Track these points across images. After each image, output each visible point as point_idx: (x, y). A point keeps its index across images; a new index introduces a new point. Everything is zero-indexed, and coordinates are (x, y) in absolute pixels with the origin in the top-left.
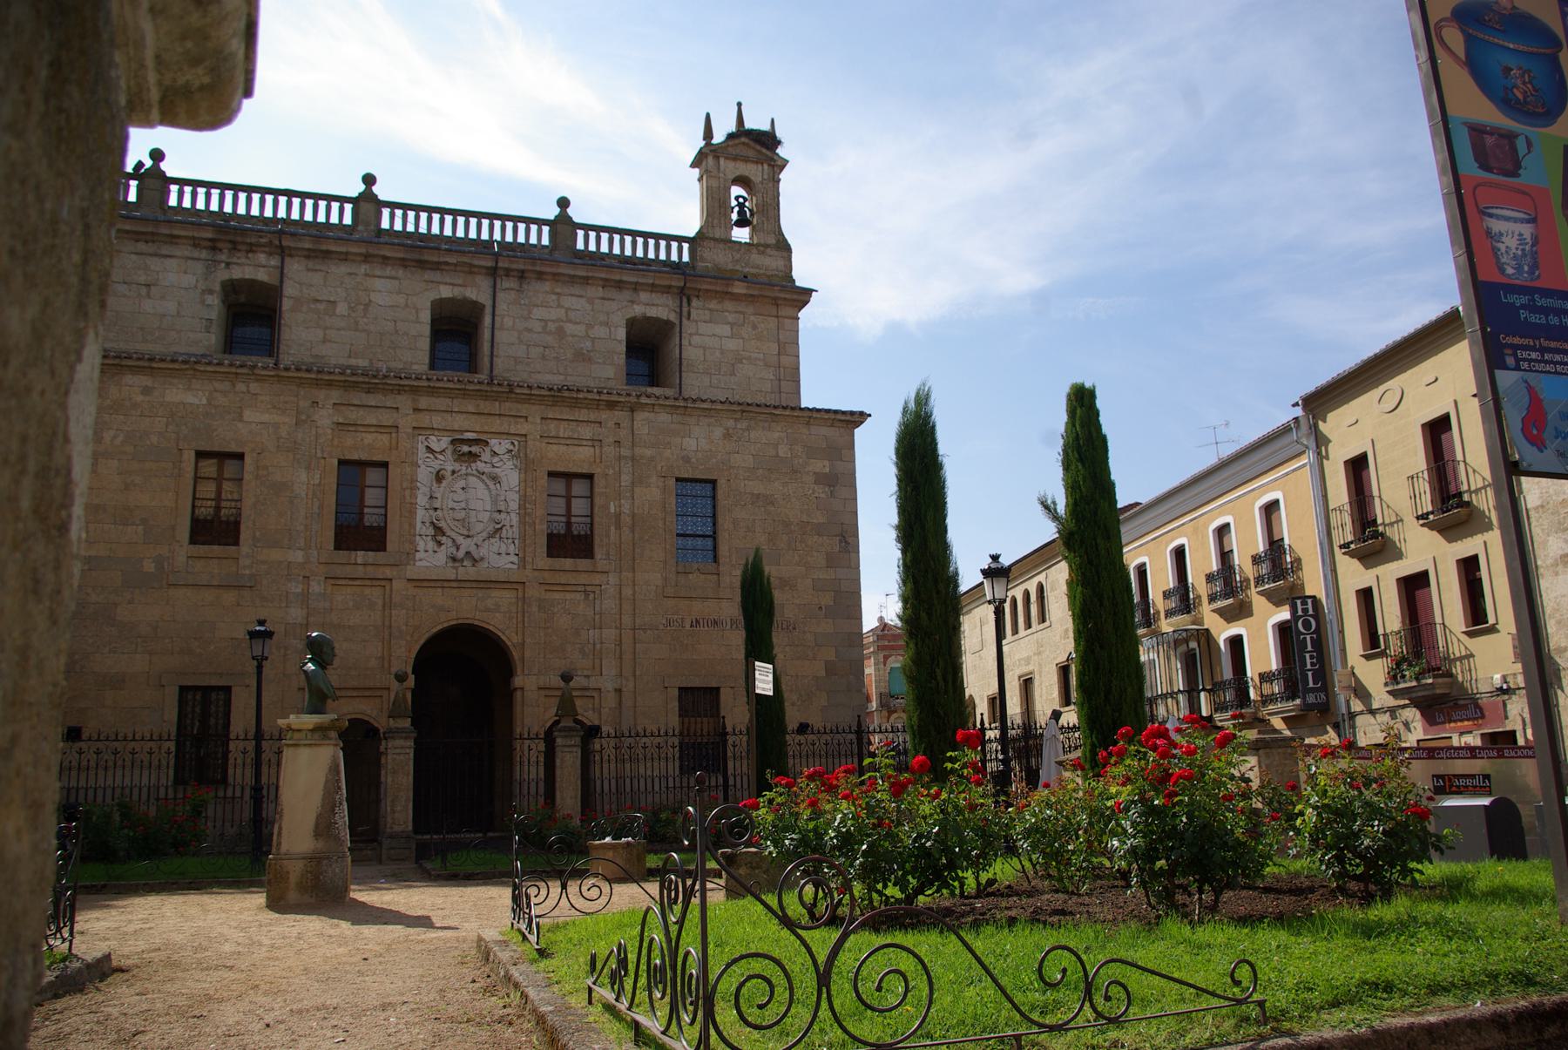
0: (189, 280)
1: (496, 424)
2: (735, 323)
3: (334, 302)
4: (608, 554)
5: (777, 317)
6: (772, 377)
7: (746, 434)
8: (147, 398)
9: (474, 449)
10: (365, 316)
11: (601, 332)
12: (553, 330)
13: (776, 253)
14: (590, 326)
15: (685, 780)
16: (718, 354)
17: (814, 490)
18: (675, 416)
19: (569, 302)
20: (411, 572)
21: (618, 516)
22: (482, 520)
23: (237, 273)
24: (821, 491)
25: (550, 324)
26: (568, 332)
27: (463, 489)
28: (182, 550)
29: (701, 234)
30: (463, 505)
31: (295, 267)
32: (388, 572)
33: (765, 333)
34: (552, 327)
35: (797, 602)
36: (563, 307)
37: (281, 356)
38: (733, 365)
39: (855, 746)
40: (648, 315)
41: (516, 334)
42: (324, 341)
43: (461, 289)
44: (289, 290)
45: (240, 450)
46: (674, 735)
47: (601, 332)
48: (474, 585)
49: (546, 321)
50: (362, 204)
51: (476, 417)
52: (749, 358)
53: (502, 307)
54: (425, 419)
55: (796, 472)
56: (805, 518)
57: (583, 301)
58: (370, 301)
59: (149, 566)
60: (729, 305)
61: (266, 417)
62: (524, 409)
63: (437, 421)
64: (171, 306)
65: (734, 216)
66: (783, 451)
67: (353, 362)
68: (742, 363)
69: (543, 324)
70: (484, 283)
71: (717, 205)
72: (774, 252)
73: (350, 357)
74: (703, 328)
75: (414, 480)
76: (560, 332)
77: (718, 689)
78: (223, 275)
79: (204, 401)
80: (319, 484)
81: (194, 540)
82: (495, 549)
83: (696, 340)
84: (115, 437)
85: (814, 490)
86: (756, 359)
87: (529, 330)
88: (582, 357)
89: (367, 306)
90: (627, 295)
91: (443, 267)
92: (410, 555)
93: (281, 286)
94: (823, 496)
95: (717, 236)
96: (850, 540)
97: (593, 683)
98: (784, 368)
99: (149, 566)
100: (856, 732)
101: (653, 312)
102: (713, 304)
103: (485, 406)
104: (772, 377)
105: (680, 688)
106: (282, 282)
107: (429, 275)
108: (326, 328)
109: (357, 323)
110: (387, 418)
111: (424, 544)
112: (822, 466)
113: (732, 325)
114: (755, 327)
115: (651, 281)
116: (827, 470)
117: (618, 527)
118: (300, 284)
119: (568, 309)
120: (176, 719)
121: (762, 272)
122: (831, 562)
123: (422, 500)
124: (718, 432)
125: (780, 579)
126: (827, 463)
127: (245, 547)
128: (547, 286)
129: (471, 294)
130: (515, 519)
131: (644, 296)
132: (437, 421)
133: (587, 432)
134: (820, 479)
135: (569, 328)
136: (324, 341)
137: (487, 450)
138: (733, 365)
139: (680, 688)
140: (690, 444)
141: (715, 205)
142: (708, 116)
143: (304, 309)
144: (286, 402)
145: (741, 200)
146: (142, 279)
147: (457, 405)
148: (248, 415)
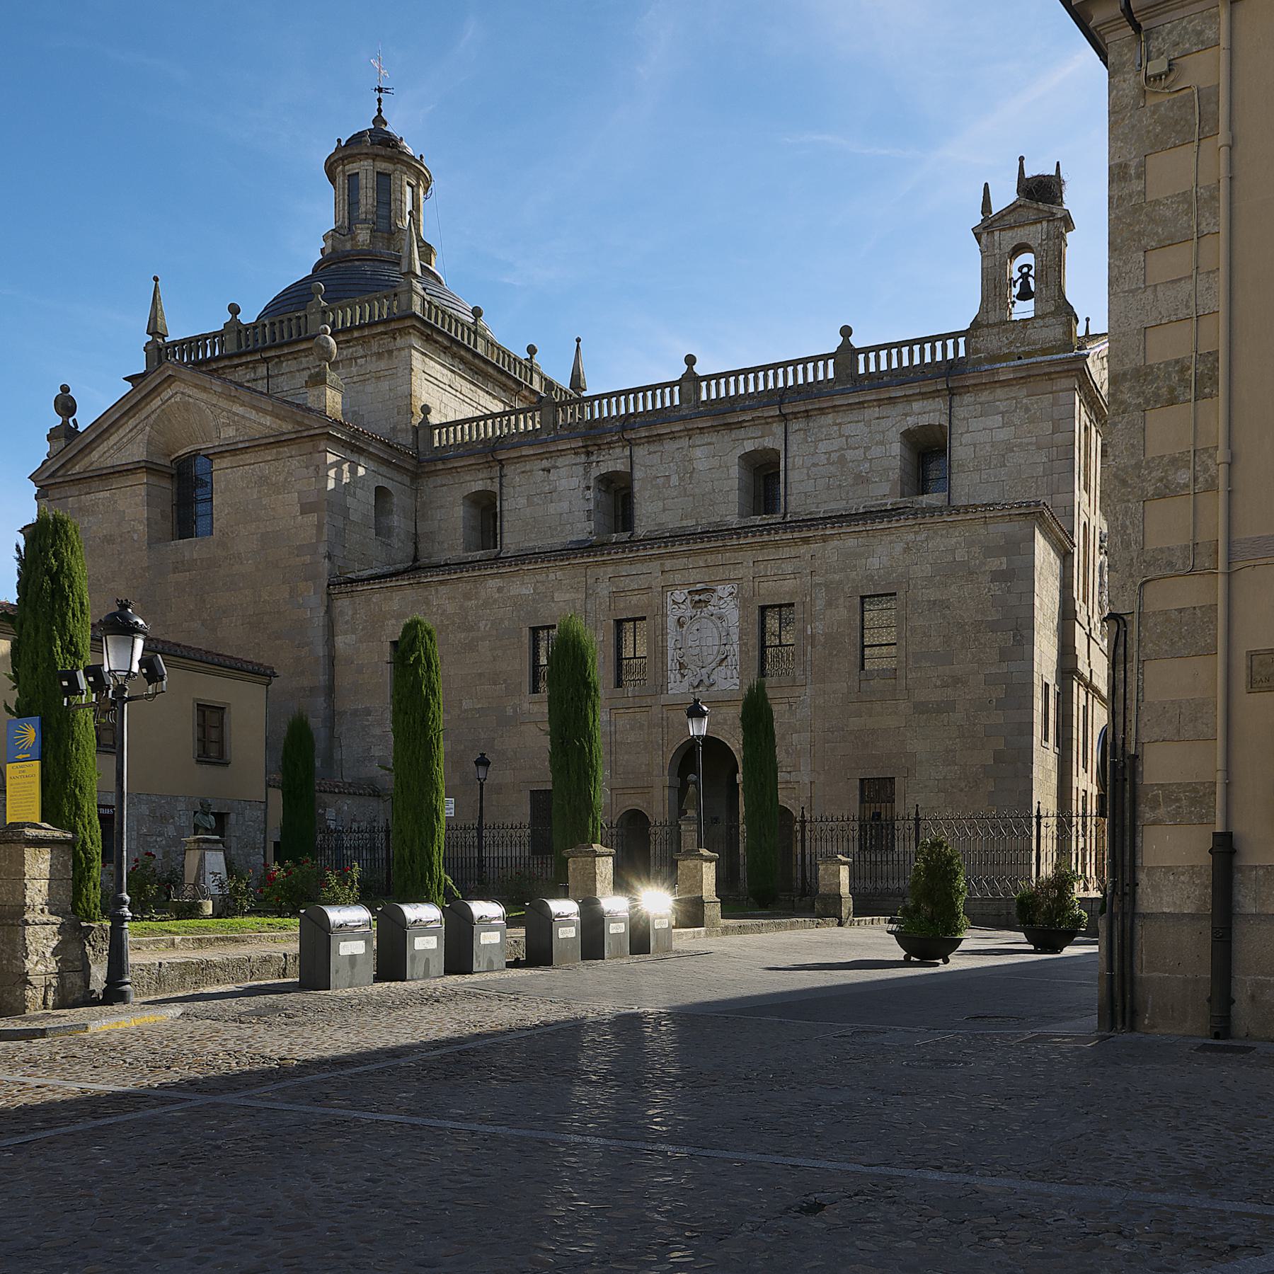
1: (721, 573)
5: (1051, 393)
8: (501, 595)
14: (867, 448)
15: (862, 856)
17: (990, 589)
18: (860, 539)
19: (849, 429)
20: (663, 699)
21: (813, 636)
24: (996, 588)
26: (849, 458)
27: (698, 630)
29: (976, 324)
31: (640, 452)
32: (649, 701)
34: (834, 456)
36: (844, 435)
37: (636, 529)
38: (1003, 456)
39: (476, 840)
42: (664, 510)
44: (638, 474)
46: (853, 820)
47: (876, 451)
49: (829, 453)
51: (706, 569)
52: (1020, 445)
53: (793, 449)
54: (671, 578)
55: (971, 573)
56: (979, 618)
58: (694, 468)
60: (1000, 393)
61: (567, 596)
62: (739, 556)
63: (678, 578)
64: (565, 505)
67: (684, 523)
68: (1013, 451)
70: (778, 429)
72: (1051, 320)
74: (975, 424)
75: (664, 628)
76: (842, 461)
79: (532, 592)
80: (603, 641)
83: (967, 438)
84: (486, 625)
85: (990, 589)
86: (1028, 444)
88: (861, 480)
90: (900, 408)
91: (745, 424)
92: (663, 687)
96: (1024, 632)
97: (793, 777)
100: (915, 819)
101: (925, 420)
103: (711, 559)
105: (862, 780)
106: (632, 469)
108: (665, 499)
110: (643, 582)
111: (673, 676)
112: (1000, 563)
114: (1027, 410)
115: (918, 390)
118: (646, 467)
122: (1004, 656)
123: (671, 644)
124: (899, 547)
128: (829, 419)
129: (768, 443)
131: (916, 406)
132: (678, 578)
133: (788, 567)
134: (998, 576)
135: (850, 455)
136: (664, 510)
138: (1003, 456)
140: (874, 563)
141: (994, 286)
144: (578, 583)
145: (1025, 270)
146: (547, 489)
147: (691, 562)
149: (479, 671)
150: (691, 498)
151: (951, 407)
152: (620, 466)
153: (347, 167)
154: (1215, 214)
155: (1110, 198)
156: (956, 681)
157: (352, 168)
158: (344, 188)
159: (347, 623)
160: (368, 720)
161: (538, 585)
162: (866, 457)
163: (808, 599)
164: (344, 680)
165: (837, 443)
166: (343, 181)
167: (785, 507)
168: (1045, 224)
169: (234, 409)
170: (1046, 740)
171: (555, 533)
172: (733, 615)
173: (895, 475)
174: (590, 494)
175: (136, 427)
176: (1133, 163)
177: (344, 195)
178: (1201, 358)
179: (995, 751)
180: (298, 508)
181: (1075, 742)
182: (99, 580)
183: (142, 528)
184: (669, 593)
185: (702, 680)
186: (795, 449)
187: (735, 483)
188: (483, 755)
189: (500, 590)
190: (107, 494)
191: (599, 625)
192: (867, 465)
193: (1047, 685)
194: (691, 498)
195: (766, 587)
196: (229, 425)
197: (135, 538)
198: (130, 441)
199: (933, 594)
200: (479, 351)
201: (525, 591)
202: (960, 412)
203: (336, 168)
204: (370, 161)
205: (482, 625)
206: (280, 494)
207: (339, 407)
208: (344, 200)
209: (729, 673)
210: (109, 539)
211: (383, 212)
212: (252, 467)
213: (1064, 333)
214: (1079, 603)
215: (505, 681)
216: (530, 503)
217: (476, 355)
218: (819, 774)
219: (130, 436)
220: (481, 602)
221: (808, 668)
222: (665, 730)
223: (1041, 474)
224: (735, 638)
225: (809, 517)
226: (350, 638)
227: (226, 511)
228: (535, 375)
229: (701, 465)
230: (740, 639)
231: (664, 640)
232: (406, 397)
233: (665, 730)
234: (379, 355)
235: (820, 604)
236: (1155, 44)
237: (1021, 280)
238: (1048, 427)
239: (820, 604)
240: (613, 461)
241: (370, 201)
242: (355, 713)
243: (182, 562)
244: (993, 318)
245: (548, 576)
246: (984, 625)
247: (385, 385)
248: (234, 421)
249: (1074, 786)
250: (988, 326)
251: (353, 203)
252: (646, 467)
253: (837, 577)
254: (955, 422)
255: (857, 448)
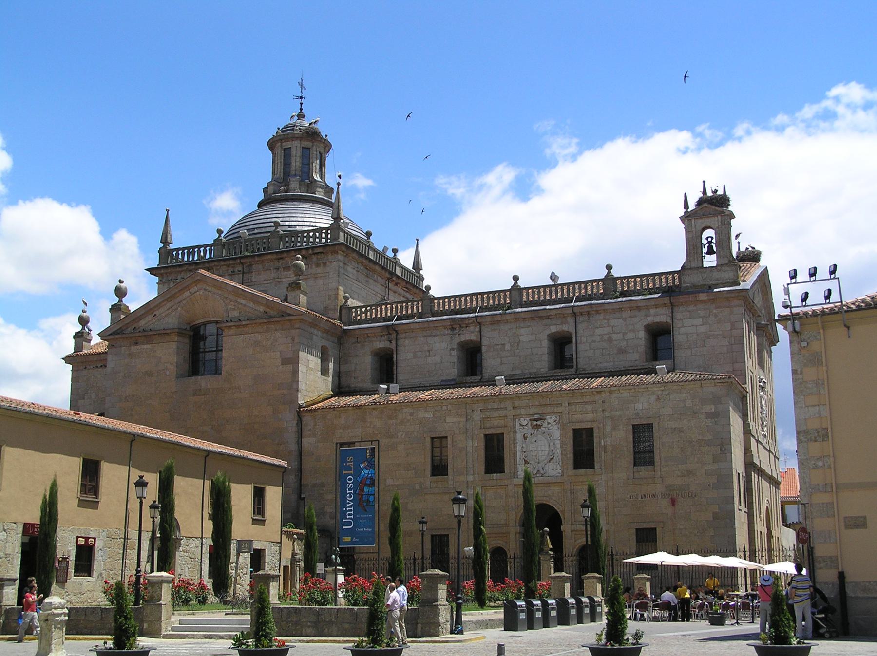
0: (444, 345)
1: (548, 409)
2: (704, 316)
3: (504, 344)
4: (601, 465)
6: (728, 344)
7: (668, 397)
9: (539, 423)
10: (518, 349)
11: (630, 335)
12: (606, 339)
13: (728, 269)
14: (625, 334)
16: (695, 336)
19: (613, 322)
22: (543, 456)
23: (463, 338)
24: (709, 422)
25: (604, 336)
28: (428, 479)
30: (536, 449)
32: (506, 482)
33: (723, 318)
34: (606, 337)
35: (697, 482)
37: (483, 375)
38: (704, 341)
40: (655, 321)
41: (588, 345)
42: (501, 364)
43: (561, 326)
44: (485, 342)
45: (446, 435)
47: (630, 335)
48: (542, 485)
50: (512, 292)
53: (580, 332)
54: (518, 411)
55: (696, 413)
57: (621, 320)
59: (417, 487)
60: (700, 306)
61: (455, 420)
64: (438, 359)
65: (705, 250)
66: (688, 403)
67: (514, 372)
69: (601, 337)
71: (692, 248)
73: (513, 370)
74: (687, 323)
75: (515, 440)
76: (610, 340)
77: (656, 529)
78: (457, 340)
79: (432, 416)
81: (433, 475)
82: (552, 468)
83: (683, 330)
86: (717, 335)
87: (594, 342)
88: (622, 351)
89: (518, 343)
93: (734, 139)
94: (710, 424)
95: (693, 266)
98: (734, 337)
99: (417, 487)
101: (658, 319)
102: (691, 308)
104: (728, 344)
105: (637, 529)
107: (545, 322)
108: (501, 358)
109: (514, 353)
112: (710, 408)
113: (702, 317)
114: (716, 316)
116: (713, 410)
117: (605, 452)
118: (489, 338)
119: (613, 327)
120: (430, 547)
121: (720, 282)
122: (715, 460)
123: (519, 448)
125: (687, 471)
126: (713, 407)
127: (450, 476)
130: (559, 452)
131: (652, 311)
132: (523, 411)
134: (710, 415)
135: (614, 337)
136: (501, 364)
137: (546, 421)
139: (637, 529)
140: (639, 406)
141: (694, 246)
142: (685, 194)
143: (492, 350)
145: (710, 239)
148: (448, 419)
149: (398, 462)
150: (518, 358)
151: (672, 312)
152: (474, 338)
153: (283, 144)
154: (824, 388)
155: (793, 379)
156: (690, 473)
157: (287, 145)
158: (281, 156)
159: (310, 430)
160: (323, 490)
161: (436, 412)
162: (624, 339)
163: (602, 425)
164: (308, 464)
165: (607, 330)
166: (281, 152)
167: (577, 365)
168: (719, 217)
169: (239, 301)
170: (740, 505)
171: (431, 375)
172: (557, 433)
173: (642, 349)
174: (454, 353)
175: (172, 307)
176: (799, 370)
177: (281, 159)
178: (824, 429)
179: (714, 513)
180: (279, 361)
181: (754, 504)
182: (141, 398)
183: (172, 368)
184: (517, 420)
185: (539, 471)
186: (582, 332)
187: (546, 350)
188: (423, 518)
189: (411, 414)
190: (149, 346)
191: (474, 437)
192: (625, 343)
193: (739, 474)
194: (518, 358)
195: (578, 417)
196: (234, 309)
197: (168, 374)
198: (167, 315)
199: (673, 424)
200: (370, 257)
201: (427, 416)
202: (678, 315)
203: (276, 144)
204: (299, 141)
205: (399, 435)
206: (268, 352)
207: (306, 302)
208: (281, 162)
209: (555, 466)
210: (149, 374)
211: (306, 170)
212: (250, 335)
213: (734, 275)
214: (752, 423)
215: (415, 469)
216: (415, 357)
217: (370, 260)
218: (612, 525)
219: (167, 312)
220: (399, 421)
221: (603, 465)
222: (516, 499)
223: (726, 352)
224: (559, 446)
225: (591, 371)
226: (312, 440)
227: (231, 361)
228: (397, 268)
229: (524, 339)
230: (561, 447)
231: (515, 447)
232: (335, 290)
233: (516, 499)
234: (318, 265)
235: (608, 428)
236: (803, 337)
237: (708, 245)
238: (728, 326)
239: (608, 428)
240: (470, 335)
241: (298, 164)
242: (314, 485)
243: (200, 390)
244: (694, 264)
245: (442, 408)
246: (703, 442)
247: (320, 282)
248: (238, 308)
249: (756, 530)
250: (691, 269)
251: (287, 164)
252: (489, 338)
253: (618, 413)
254: (675, 321)
255: (619, 333)
